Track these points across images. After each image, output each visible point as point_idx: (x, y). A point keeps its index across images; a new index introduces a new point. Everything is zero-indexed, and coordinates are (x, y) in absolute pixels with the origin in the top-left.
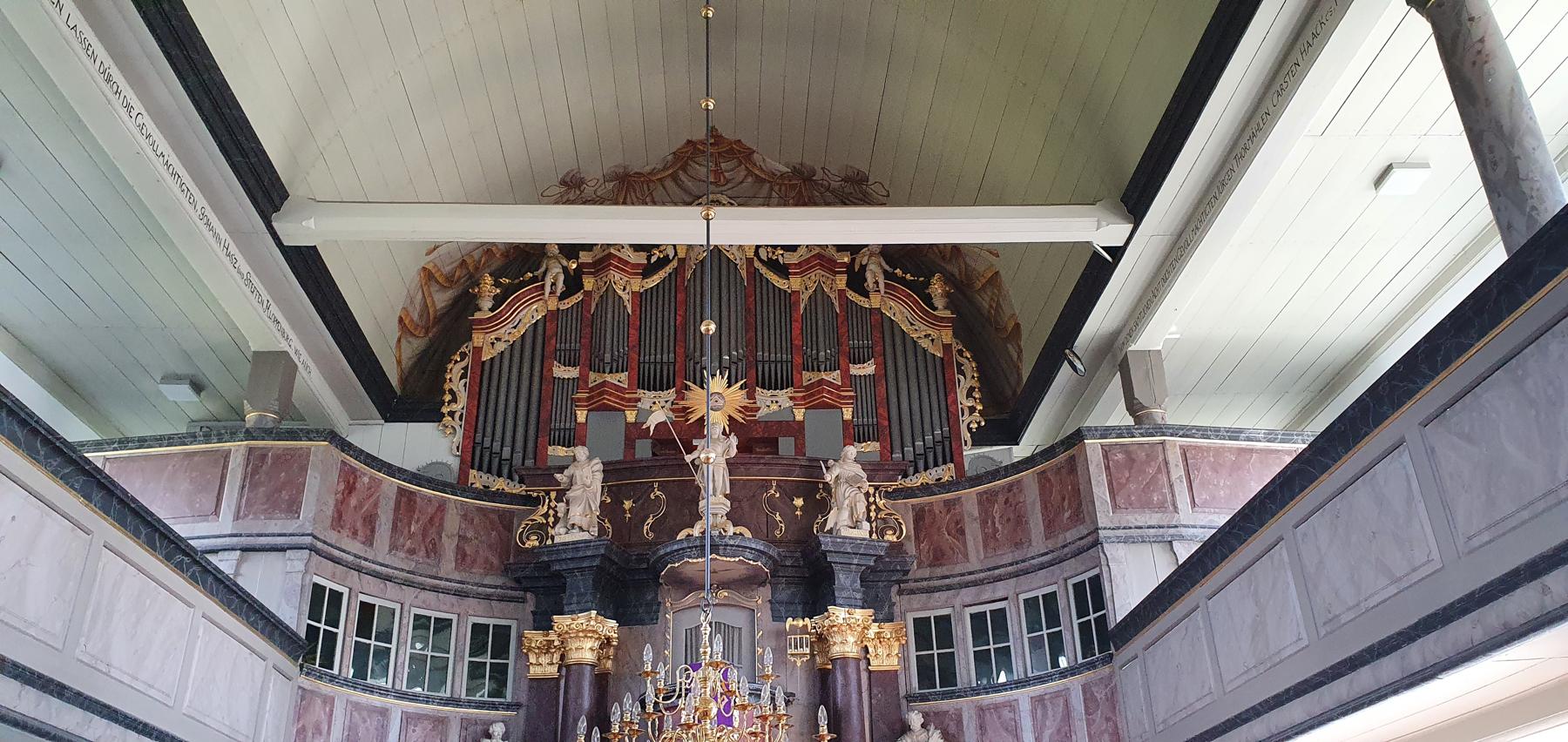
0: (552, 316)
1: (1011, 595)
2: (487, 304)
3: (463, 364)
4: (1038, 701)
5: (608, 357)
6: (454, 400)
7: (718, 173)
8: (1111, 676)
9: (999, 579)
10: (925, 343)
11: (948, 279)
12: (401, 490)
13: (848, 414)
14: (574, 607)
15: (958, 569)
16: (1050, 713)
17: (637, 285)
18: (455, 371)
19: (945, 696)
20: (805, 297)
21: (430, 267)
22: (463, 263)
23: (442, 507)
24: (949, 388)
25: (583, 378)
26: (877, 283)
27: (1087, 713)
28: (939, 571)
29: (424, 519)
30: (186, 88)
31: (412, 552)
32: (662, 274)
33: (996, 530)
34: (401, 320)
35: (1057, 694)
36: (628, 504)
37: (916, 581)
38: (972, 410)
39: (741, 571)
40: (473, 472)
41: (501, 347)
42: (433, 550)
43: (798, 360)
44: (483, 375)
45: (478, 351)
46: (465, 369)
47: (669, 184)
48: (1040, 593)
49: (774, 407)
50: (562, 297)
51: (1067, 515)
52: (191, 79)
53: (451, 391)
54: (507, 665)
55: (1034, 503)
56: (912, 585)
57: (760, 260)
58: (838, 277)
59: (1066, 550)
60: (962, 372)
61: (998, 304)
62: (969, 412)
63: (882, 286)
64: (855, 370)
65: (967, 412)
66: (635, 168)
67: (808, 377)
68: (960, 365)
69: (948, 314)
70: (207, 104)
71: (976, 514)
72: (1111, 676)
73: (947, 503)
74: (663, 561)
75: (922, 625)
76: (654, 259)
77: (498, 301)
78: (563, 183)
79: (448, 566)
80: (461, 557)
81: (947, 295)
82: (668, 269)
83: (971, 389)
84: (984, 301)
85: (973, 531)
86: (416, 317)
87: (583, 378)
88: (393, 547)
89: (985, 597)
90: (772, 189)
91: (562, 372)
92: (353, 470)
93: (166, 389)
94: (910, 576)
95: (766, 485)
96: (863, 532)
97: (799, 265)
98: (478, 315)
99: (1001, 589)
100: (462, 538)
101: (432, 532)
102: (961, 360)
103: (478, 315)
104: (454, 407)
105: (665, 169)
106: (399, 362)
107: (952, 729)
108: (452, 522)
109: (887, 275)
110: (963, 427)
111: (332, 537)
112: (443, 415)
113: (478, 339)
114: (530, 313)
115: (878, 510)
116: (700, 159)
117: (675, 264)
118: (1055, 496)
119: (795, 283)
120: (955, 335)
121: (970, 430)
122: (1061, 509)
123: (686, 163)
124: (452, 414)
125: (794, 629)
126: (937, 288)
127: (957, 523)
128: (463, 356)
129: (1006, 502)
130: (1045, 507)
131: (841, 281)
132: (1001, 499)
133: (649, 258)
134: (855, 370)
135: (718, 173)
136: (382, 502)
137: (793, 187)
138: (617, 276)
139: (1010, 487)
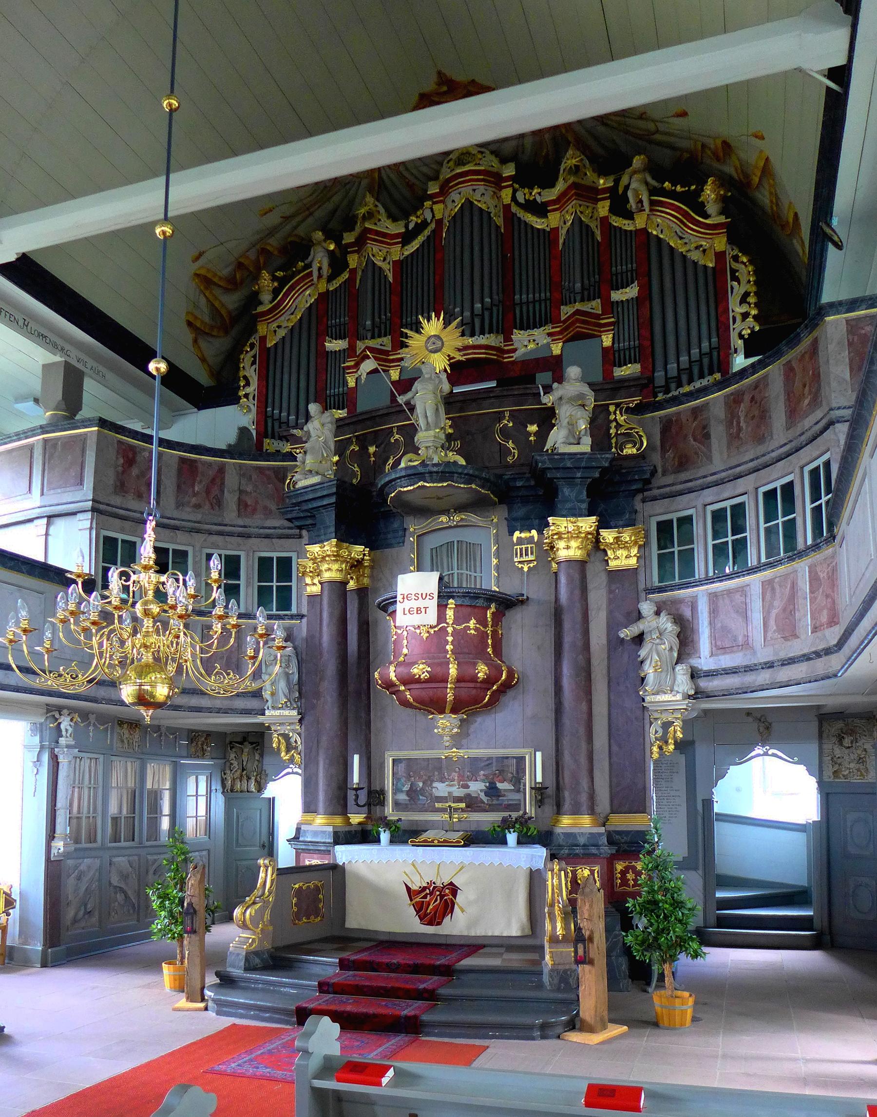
0: (324, 297)
1: (751, 488)
2: (266, 297)
3: (252, 353)
4: (768, 585)
6: (248, 384)
8: (833, 556)
9: (739, 476)
10: (695, 256)
11: (724, 181)
12: (183, 460)
13: (607, 340)
14: (323, 537)
15: (701, 473)
16: (778, 595)
17: (397, 253)
18: (246, 360)
19: (687, 586)
20: (563, 232)
21: (203, 272)
23: (222, 469)
24: (721, 297)
25: (352, 348)
27: (811, 592)
28: (684, 476)
31: (198, 506)
32: (421, 239)
33: (740, 429)
34: (190, 324)
35: (786, 576)
36: (372, 449)
37: (659, 488)
38: (745, 316)
39: (464, 498)
40: (267, 441)
41: (282, 333)
42: (218, 503)
44: (267, 360)
45: (263, 339)
46: (254, 356)
48: (778, 484)
49: (532, 346)
50: (330, 279)
51: (806, 402)
53: (245, 377)
54: (239, 585)
56: (656, 492)
57: (518, 204)
58: (600, 204)
59: (803, 438)
60: (738, 280)
61: (777, 198)
62: (742, 318)
64: (616, 296)
65: (739, 318)
67: (566, 311)
68: (733, 271)
69: (722, 219)
72: (833, 556)
74: (382, 493)
75: (664, 528)
76: (411, 226)
77: (276, 292)
79: (230, 514)
80: (243, 507)
81: (723, 199)
82: (427, 232)
83: (746, 295)
84: (764, 198)
85: (718, 432)
86: (207, 319)
87: (352, 348)
88: (179, 505)
89: (726, 495)
91: (334, 345)
92: (132, 448)
93: (20, 406)
94: (656, 482)
95: (500, 416)
96: (585, 446)
98: (260, 309)
99: (743, 484)
100: (241, 492)
101: (215, 491)
102: (735, 265)
103: (260, 309)
104: (248, 390)
106: (203, 360)
107: (687, 613)
108: (231, 480)
109: (653, 192)
110: (734, 336)
111: (117, 500)
112: (240, 398)
114: (306, 298)
115: (618, 426)
117: (433, 225)
118: (798, 384)
119: (554, 220)
120: (731, 241)
121: (741, 336)
122: (802, 396)
124: (246, 396)
125: (520, 541)
126: (709, 193)
128: (252, 346)
129: (753, 399)
131: (603, 208)
132: (747, 398)
133: (407, 226)
134: (616, 296)
139: (756, 386)
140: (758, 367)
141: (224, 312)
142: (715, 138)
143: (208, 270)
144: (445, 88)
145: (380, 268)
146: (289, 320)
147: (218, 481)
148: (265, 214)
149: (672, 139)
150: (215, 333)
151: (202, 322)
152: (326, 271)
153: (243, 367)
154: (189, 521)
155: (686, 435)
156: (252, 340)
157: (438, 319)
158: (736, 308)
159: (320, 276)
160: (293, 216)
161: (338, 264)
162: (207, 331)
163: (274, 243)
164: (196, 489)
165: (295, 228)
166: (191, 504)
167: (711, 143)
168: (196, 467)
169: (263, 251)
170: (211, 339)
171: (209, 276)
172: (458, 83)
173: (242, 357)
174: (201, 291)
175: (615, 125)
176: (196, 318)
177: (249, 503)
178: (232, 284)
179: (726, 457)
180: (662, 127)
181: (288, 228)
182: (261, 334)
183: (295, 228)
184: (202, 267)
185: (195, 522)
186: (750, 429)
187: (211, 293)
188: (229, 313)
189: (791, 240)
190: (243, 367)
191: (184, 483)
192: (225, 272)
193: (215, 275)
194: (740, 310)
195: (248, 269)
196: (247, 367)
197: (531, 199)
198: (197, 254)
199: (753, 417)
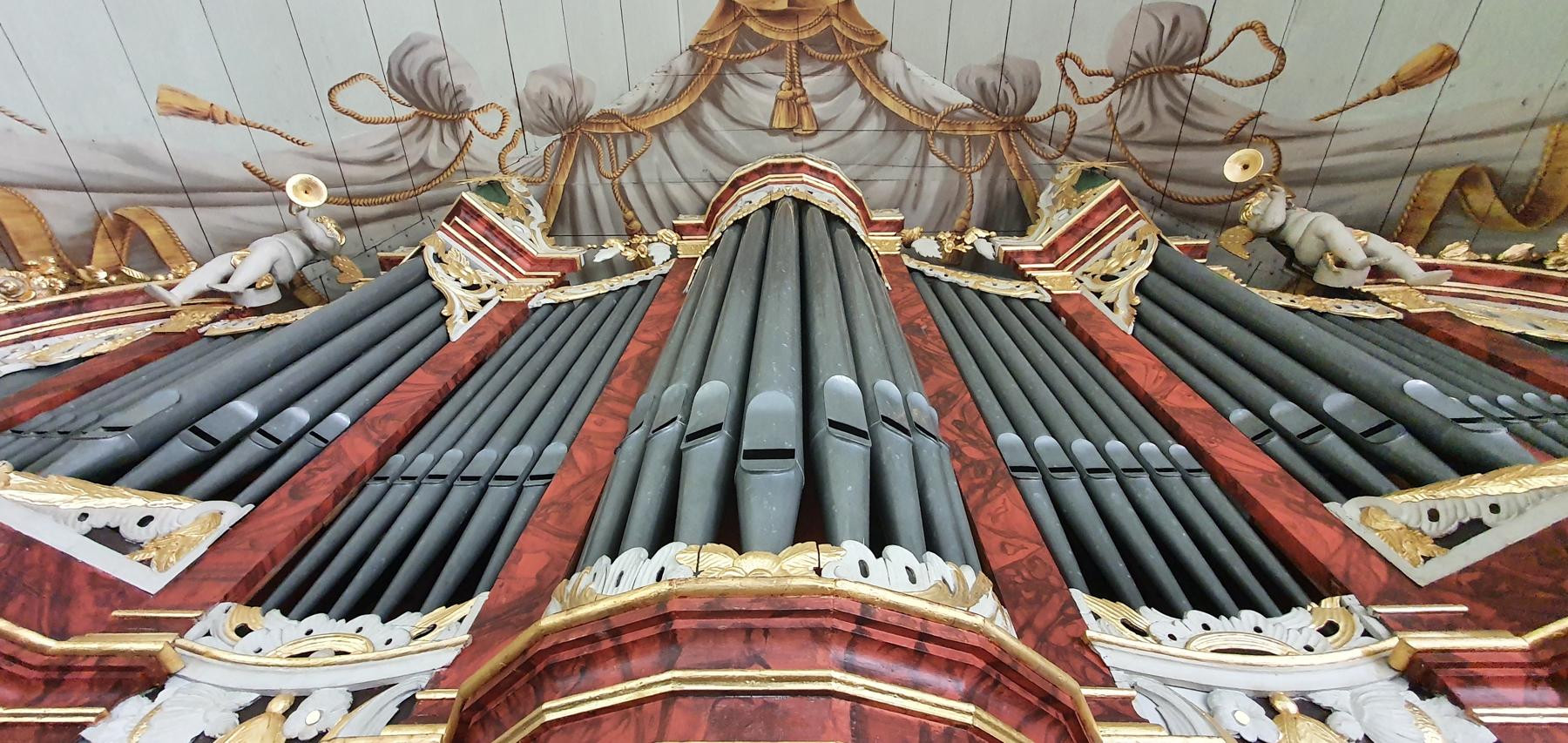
7: (795, 103)
47: (679, 138)
55: (237, 219)
66: (599, 102)
78: (400, 83)
90: (926, 148)
116: (752, 67)
123: (720, 80)
135: (795, 103)
137: (978, 143)
138: (459, 252)
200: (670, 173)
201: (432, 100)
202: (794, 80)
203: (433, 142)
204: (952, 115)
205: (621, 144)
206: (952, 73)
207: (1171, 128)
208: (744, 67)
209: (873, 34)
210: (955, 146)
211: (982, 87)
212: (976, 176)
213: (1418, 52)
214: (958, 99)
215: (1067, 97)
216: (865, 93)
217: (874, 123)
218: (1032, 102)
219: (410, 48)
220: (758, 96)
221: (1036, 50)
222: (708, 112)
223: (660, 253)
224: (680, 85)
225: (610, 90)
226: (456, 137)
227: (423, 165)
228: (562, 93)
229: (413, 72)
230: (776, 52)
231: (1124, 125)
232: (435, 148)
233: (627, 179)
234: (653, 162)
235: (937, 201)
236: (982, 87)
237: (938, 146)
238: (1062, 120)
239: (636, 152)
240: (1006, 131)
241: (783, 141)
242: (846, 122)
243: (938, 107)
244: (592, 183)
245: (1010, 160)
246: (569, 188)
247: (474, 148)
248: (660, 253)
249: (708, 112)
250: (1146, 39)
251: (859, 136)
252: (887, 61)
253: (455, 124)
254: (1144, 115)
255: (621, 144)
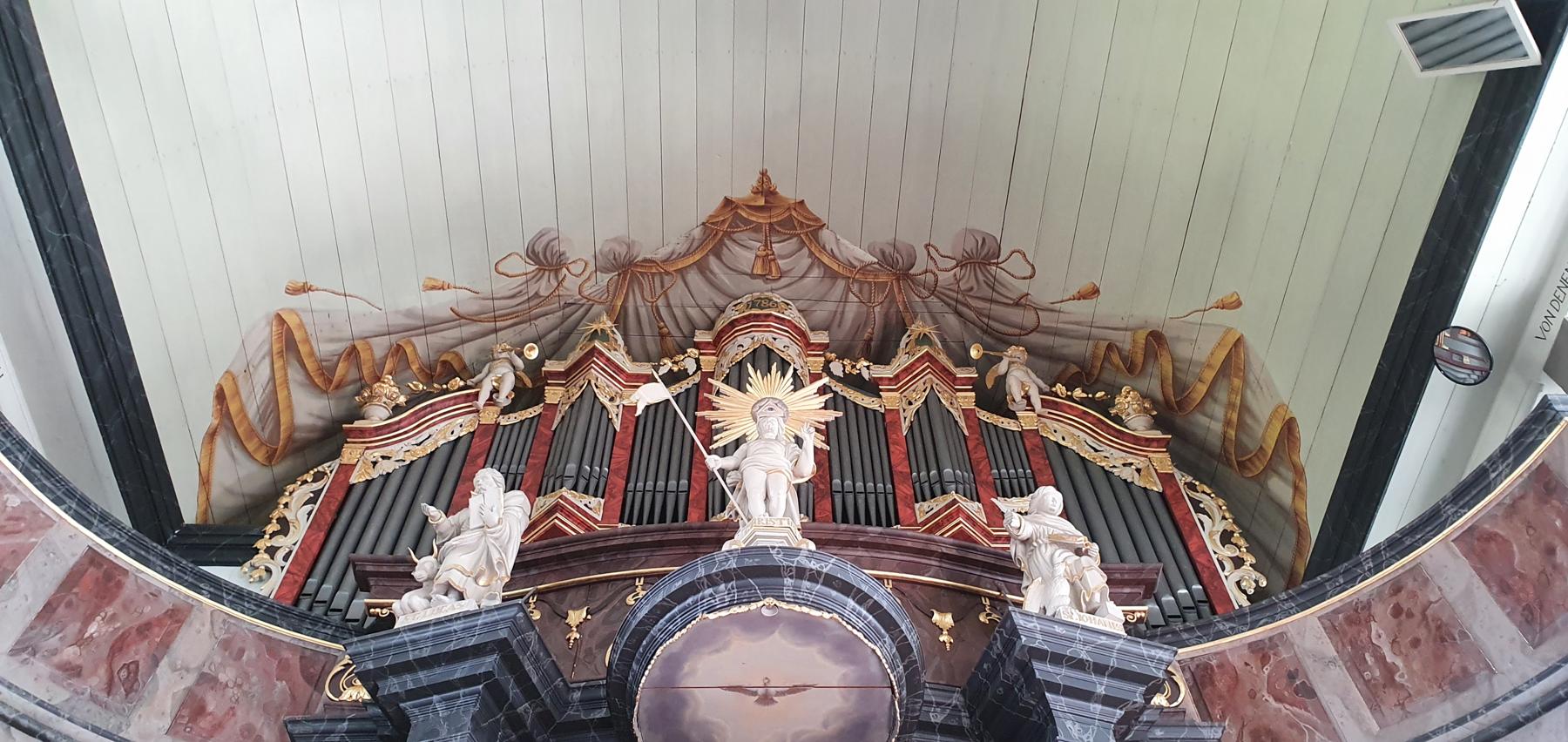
3: (316, 486)
5: (572, 468)
7: (768, 259)
12: (93, 557)
21: (292, 321)
22: (353, 353)
24: (1184, 533)
26: (1027, 397)
29: (125, 622)
30: (103, 430)
31: (72, 671)
33: (1390, 671)
34: (220, 396)
36: (576, 617)
41: (386, 467)
42: (126, 682)
43: (904, 490)
45: (347, 469)
46: (317, 493)
47: (694, 277)
50: (505, 411)
52: (78, 314)
63: (1036, 400)
65: (1229, 565)
68: (1196, 503)
70: (29, 159)
71: (1331, 651)
73: (1255, 647)
78: (532, 254)
86: (252, 411)
90: (848, 289)
97: (897, 378)
101: (139, 652)
104: (279, 541)
105: (687, 254)
106: (205, 482)
112: (257, 551)
113: (350, 453)
116: (741, 236)
123: (721, 242)
124: (272, 551)
127: (1292, 676)
129: (1397, 611)
130: (1504, 589)
131: (967, 399)
135: (768, 259)
136: (36, 558)
139: (1396, 587)
140: (1385, 555)
141: (284, 419)
142: (1134, 330)
143: (301, 325)
144: (761, 202)
145: (604, 407)
146: (404, 450)
147: (157, 635)
148: (434, 288)
149: (1058, 341)
150: (251, 446)
151: (242, 410)
152: (504, 399)
153: (286, 505)
154: (27, 695)
155: (1253, 695)
156: (325, 467)
157: (783, 375)
158: (1220, 552)
159: (491, 401)
160: (472, 319)
161: (527, 394)
162: (240, 431)
163: (422, 347)
164: (92, 629)
165: (463, 342)
166: (56, 659)
167: (1125, 341)
168: (119, 585)
169: (398, 350)
170: (237, 453)
171: (298, 336)
172: (782, 199)
173: (290, 488)
174: (271, 353)
175: (972, 315)
176: (237, 393)
177: (210, 708)
178: (323, 378)
179: (1376, 728)
180: (1047, 320)
181: (453, 334)
182: (345, 461)
183: (463, 342)
184: (292, 311)
185: (41, 704)
186: (1416, 666)
187: (284, 368)
188: (293, 428)
189: (1264, 486)
190: (286, 505)
191: (69, 605)
192: (325, 349)
193: (307, 341)
194: (1227, 552)
195: (359, 369)
196: (292, 505)
197: (855, 372)
198: (301, 281)
199: (1416, 643)
200: (689, 300)
201: (546, 259)
202: (767, 245)
203: (544, 282)
204: (865, 269)
205: (657, 280)
206: (865, 244)
207: (988, 292)
208: (735, 236)
209: (817, 220)
210: (866, 287)
211: (883, 253)
212: (877, 309)
213: (1082, 284)
214: (870, 258)
215: (931, 266)
216: (811, 254)
217: (816, 272)
218: (913, 265)
219: (541, 235)
220: (745, 254)
221: (912, 237)
222: (713, 262)
223: (691, 366)
224: (696, 244)
225: (650, 247)
226: (556, 277)
227: (537, 295)
228: (623, 250)
229: (539, 248)
230: (757, 228)
231: (963, 286)
232: (544, 286)
233: (661, 303)
234: (677, 293)
235: (854, 320)
236: (883, 253)
237: (855, 288)
238: (930, 277)
239: (667, 285)
240: (898, 280)
241: (759, 283)
242: (798, 272)
243: (856, 263)
244: (638, 303)
245: (899, 298)
246: (624, 307)
247: (565, 284)
248: (691, 366)
249: (713, 262)
250: (970, 245)
251: (806, 281)
252: (825, 234)
253: (557, 272)
254: (973, 282)
255: (657, 280)
